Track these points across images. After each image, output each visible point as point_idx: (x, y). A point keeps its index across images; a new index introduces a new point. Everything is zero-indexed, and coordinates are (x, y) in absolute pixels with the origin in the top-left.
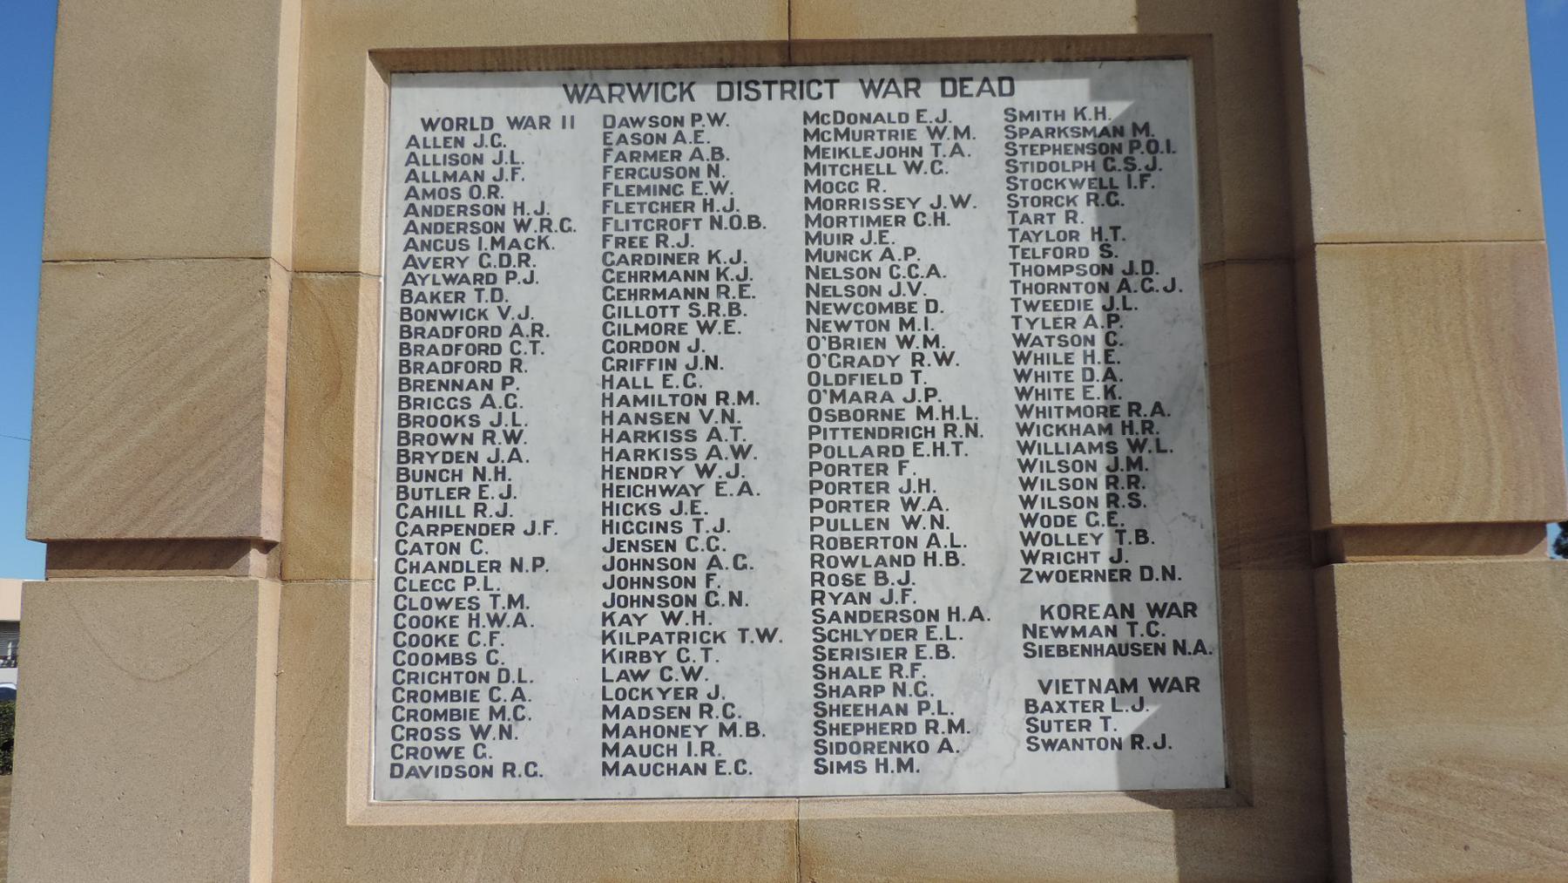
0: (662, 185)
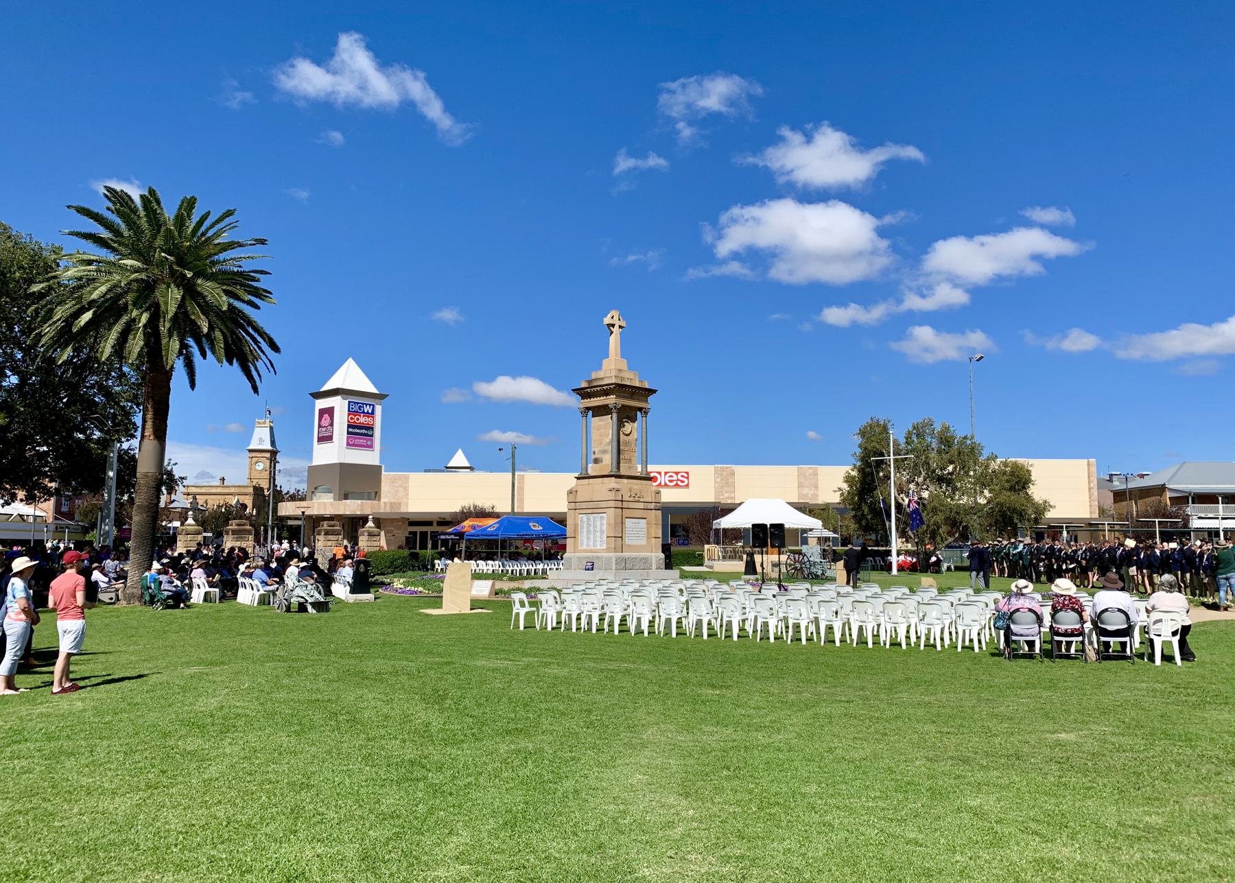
0: (588, 519)
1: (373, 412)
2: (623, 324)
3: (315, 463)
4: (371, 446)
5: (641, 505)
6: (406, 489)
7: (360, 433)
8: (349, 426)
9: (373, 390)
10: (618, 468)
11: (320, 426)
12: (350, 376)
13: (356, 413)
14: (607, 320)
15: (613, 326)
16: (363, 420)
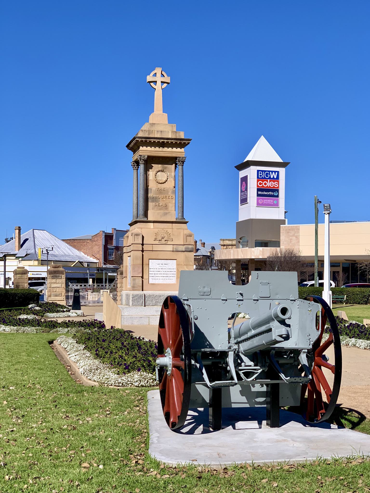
1: (278, 177)
2: (167, 79)
3: (240, 220)
4: (277, 205)
5: (170, 248)
6: (297, 238)
7: (267, 194)
8: (258, 190)
9: (279, 160)
10: (146, 215)
11: (241, 192)
12: (263, 150)
13: (263, 179)
14: (149, 78)
15: (155, 82)
16: (269, 184)
